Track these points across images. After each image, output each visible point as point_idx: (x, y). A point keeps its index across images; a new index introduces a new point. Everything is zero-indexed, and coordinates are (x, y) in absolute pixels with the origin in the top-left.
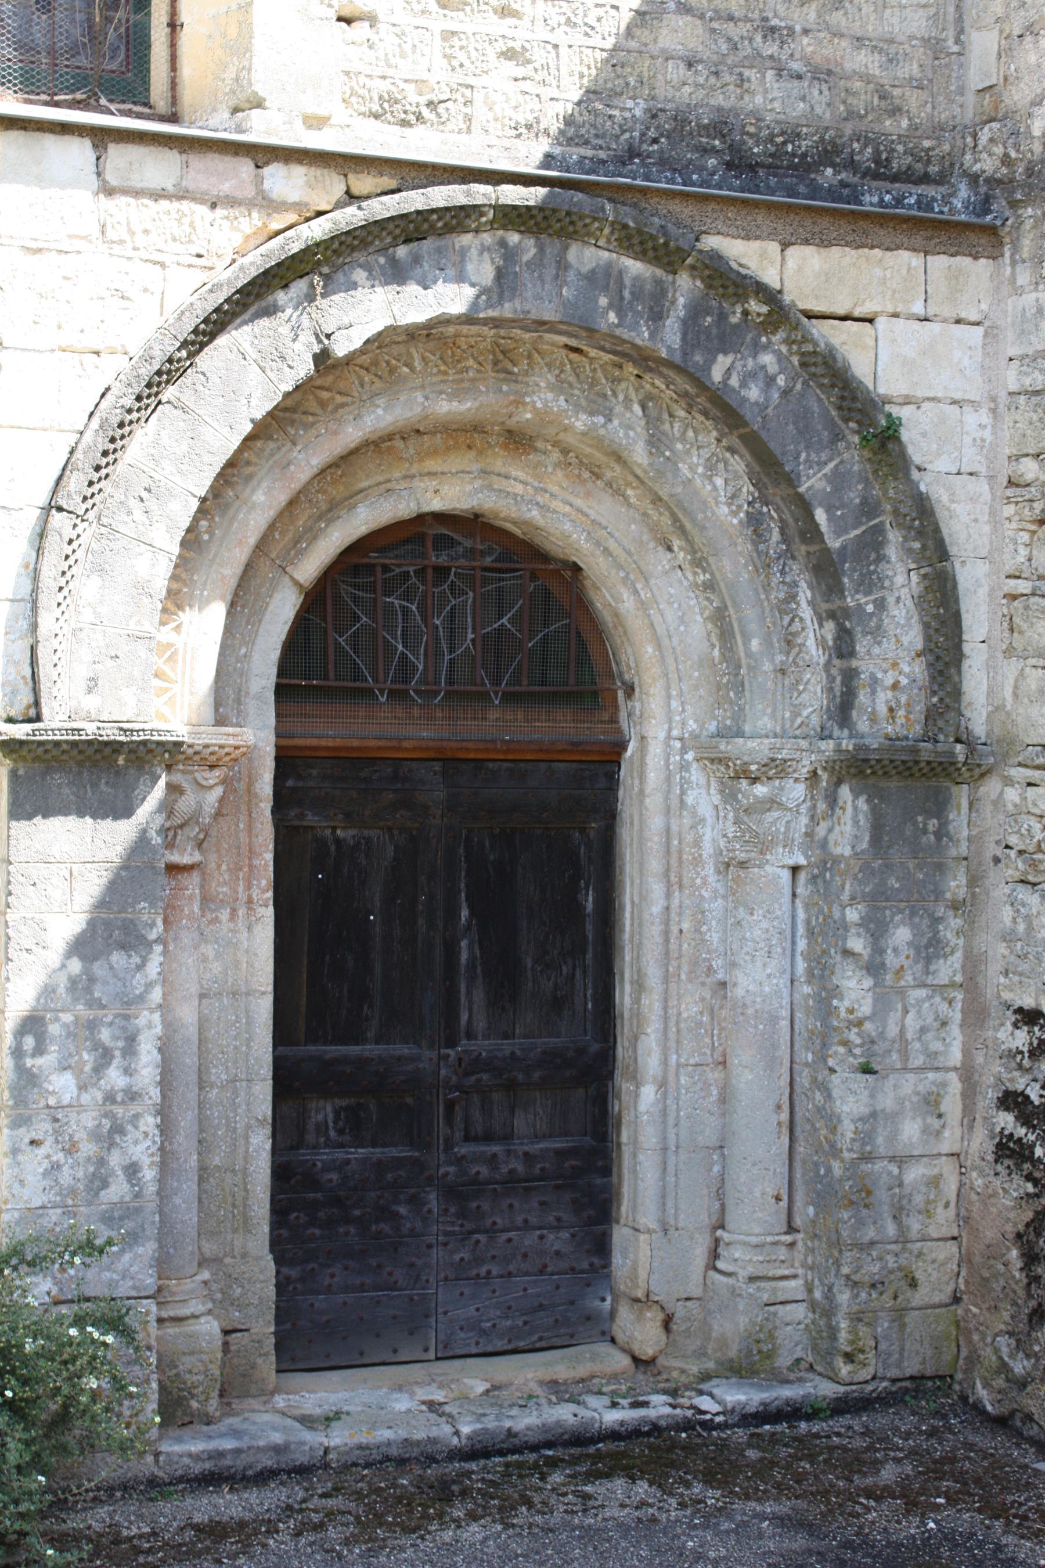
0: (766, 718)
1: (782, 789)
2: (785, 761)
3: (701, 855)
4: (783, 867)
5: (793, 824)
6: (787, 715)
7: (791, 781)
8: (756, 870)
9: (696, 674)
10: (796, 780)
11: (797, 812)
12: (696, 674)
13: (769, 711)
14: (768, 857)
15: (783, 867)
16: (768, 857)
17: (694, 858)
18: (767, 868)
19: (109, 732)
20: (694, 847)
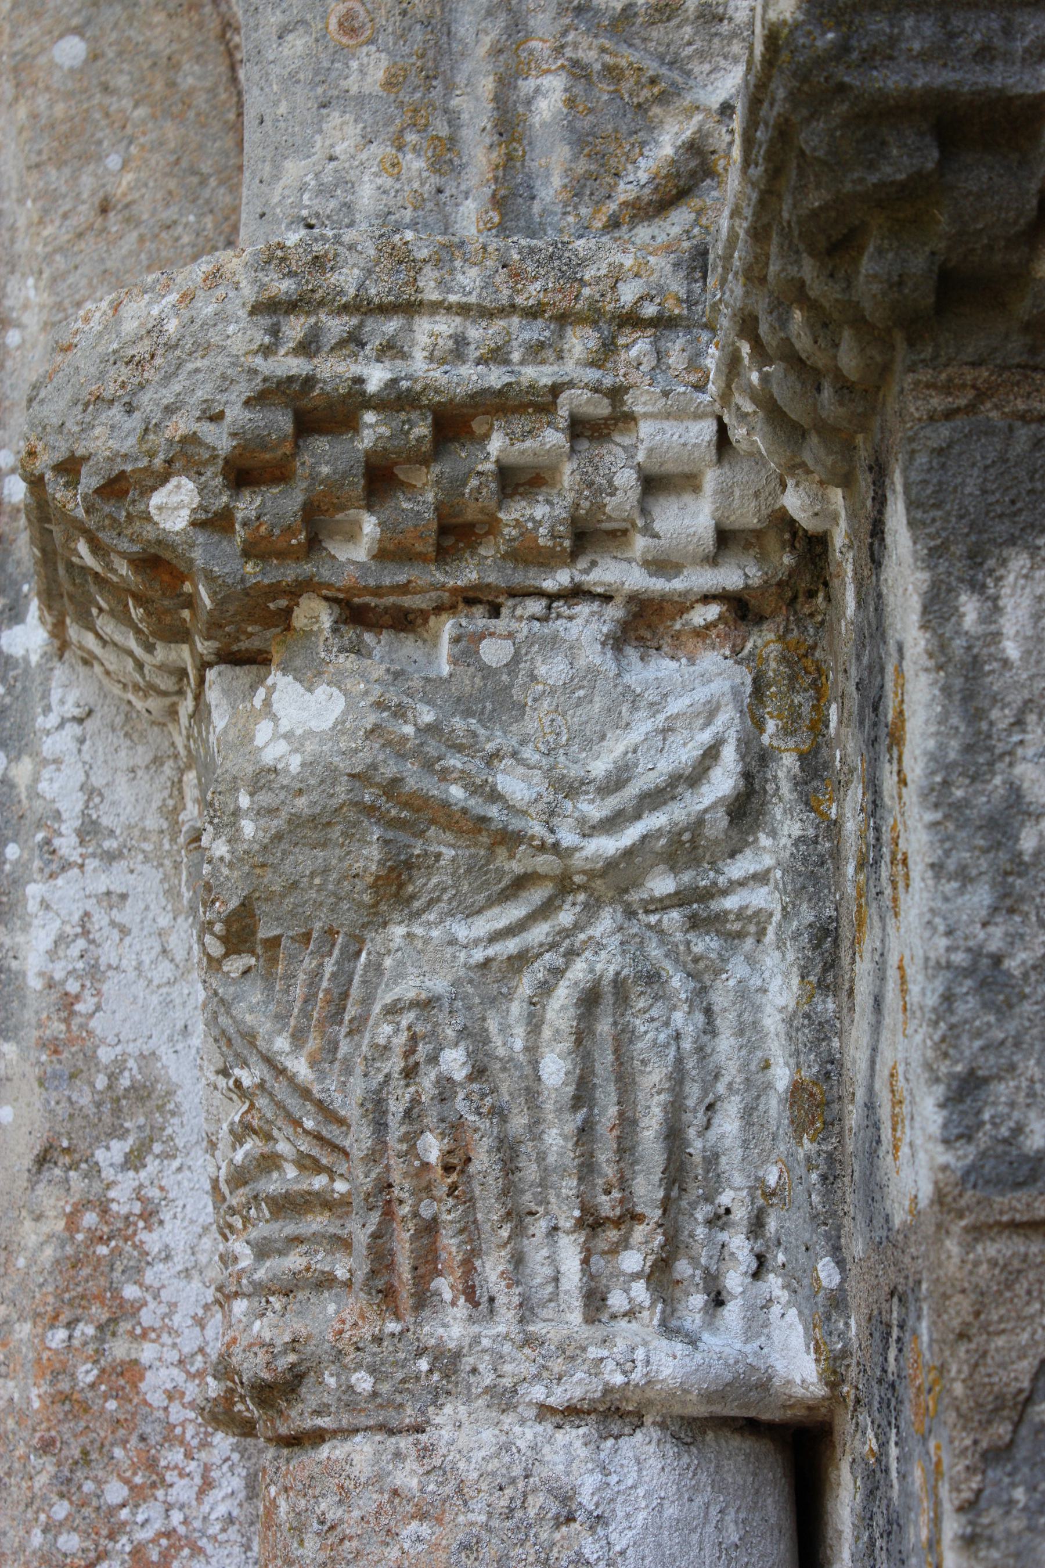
0: (342, 133)
1: (496, 698)
2: (454, 423)
3: (131, 1371)
4: (612, 1413)
5: (659, 1028)
6: (548, 98)
7: (586, 628)
8: (361, 1453)
9: (71, 51)
10: (644, 624)
11: (698, 906)
12: (71, 51)
13: (369, 70)
14: (452, 1326)
15: (612, 1413)
16: (452, 1326)
17: (70, 1403)
18: (466, 1435)
19: (906, 1173)
20: (66, 1310)
